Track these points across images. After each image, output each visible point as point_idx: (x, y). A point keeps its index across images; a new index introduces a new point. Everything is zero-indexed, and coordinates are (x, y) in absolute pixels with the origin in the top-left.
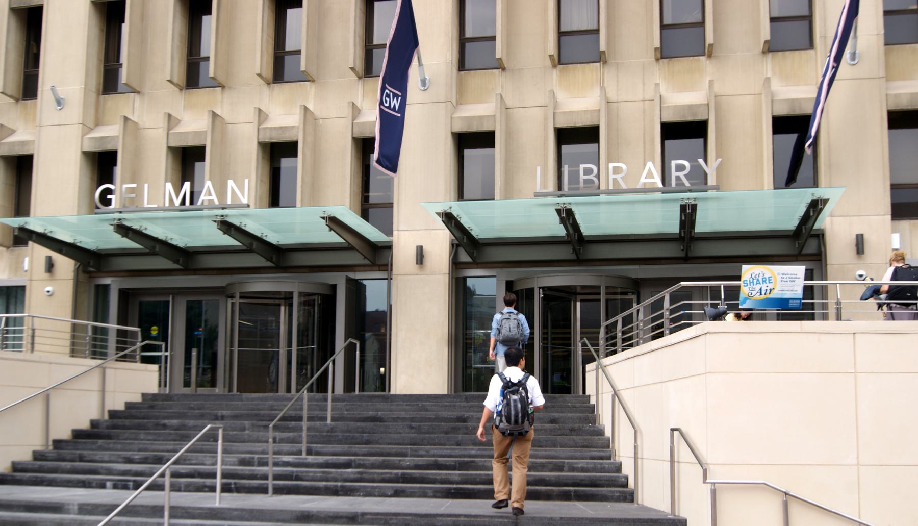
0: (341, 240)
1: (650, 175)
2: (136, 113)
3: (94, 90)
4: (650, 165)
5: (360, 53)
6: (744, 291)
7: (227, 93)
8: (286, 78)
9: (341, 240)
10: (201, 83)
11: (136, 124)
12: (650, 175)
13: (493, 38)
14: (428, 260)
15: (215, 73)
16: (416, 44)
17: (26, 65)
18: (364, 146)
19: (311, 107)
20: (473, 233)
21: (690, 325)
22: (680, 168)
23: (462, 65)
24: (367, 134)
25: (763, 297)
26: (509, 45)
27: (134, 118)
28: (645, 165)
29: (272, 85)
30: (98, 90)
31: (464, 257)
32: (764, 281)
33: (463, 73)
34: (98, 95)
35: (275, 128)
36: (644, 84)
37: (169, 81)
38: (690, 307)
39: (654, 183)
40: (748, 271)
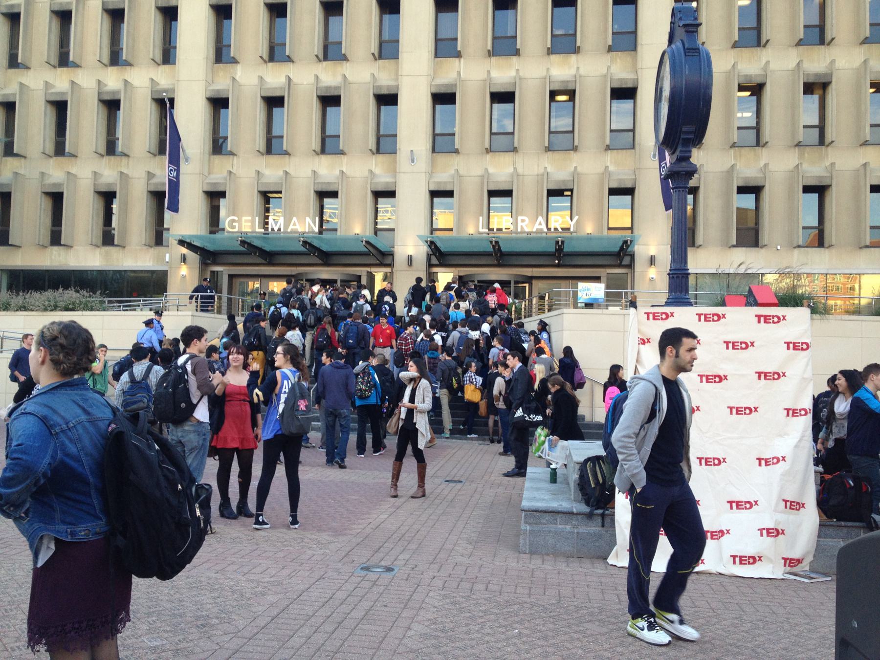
0: (366, 250)
1: (540, 224)
2: (234, 168)
3: (208, 152)
4: (540, 218)
5: (319, 140)
6: (580, 294)
7: (292, 158)
8: (273, 151)
9: (366, 250)
10: (223, 152)
11: (235, 174)
12: (540, 224)
13: (282, 137)
14: (414, 263)
15: (287, 147)
16: (180, 140)
17: (160, 134)
18: (157, 196)
19: (344, 170)
20: (441, 249)
21: (560, 309)
22: (523, 221)
23: (434, 151)
24: (160, 189)
25: (588, 297)
26: (461, 139)
27: (234, 171)
28: (537, 218)
29: (320, 156)
30: (209, 153)
31: (434, 261)
32: (588, 290)
33: (435, 154)
34: (210, 155)
35: (324, 183)
36: (538, 166)
37: (258, 151)
38: (560, 300)
39: (542, 229)
40: (581, 285)
